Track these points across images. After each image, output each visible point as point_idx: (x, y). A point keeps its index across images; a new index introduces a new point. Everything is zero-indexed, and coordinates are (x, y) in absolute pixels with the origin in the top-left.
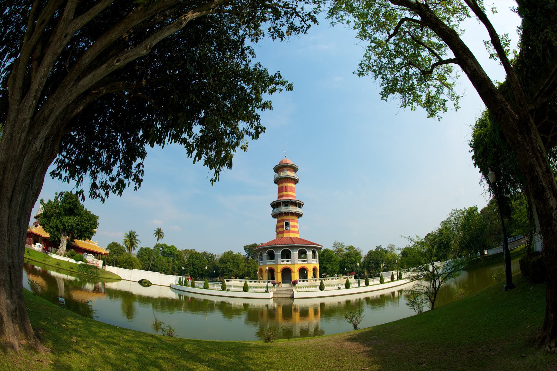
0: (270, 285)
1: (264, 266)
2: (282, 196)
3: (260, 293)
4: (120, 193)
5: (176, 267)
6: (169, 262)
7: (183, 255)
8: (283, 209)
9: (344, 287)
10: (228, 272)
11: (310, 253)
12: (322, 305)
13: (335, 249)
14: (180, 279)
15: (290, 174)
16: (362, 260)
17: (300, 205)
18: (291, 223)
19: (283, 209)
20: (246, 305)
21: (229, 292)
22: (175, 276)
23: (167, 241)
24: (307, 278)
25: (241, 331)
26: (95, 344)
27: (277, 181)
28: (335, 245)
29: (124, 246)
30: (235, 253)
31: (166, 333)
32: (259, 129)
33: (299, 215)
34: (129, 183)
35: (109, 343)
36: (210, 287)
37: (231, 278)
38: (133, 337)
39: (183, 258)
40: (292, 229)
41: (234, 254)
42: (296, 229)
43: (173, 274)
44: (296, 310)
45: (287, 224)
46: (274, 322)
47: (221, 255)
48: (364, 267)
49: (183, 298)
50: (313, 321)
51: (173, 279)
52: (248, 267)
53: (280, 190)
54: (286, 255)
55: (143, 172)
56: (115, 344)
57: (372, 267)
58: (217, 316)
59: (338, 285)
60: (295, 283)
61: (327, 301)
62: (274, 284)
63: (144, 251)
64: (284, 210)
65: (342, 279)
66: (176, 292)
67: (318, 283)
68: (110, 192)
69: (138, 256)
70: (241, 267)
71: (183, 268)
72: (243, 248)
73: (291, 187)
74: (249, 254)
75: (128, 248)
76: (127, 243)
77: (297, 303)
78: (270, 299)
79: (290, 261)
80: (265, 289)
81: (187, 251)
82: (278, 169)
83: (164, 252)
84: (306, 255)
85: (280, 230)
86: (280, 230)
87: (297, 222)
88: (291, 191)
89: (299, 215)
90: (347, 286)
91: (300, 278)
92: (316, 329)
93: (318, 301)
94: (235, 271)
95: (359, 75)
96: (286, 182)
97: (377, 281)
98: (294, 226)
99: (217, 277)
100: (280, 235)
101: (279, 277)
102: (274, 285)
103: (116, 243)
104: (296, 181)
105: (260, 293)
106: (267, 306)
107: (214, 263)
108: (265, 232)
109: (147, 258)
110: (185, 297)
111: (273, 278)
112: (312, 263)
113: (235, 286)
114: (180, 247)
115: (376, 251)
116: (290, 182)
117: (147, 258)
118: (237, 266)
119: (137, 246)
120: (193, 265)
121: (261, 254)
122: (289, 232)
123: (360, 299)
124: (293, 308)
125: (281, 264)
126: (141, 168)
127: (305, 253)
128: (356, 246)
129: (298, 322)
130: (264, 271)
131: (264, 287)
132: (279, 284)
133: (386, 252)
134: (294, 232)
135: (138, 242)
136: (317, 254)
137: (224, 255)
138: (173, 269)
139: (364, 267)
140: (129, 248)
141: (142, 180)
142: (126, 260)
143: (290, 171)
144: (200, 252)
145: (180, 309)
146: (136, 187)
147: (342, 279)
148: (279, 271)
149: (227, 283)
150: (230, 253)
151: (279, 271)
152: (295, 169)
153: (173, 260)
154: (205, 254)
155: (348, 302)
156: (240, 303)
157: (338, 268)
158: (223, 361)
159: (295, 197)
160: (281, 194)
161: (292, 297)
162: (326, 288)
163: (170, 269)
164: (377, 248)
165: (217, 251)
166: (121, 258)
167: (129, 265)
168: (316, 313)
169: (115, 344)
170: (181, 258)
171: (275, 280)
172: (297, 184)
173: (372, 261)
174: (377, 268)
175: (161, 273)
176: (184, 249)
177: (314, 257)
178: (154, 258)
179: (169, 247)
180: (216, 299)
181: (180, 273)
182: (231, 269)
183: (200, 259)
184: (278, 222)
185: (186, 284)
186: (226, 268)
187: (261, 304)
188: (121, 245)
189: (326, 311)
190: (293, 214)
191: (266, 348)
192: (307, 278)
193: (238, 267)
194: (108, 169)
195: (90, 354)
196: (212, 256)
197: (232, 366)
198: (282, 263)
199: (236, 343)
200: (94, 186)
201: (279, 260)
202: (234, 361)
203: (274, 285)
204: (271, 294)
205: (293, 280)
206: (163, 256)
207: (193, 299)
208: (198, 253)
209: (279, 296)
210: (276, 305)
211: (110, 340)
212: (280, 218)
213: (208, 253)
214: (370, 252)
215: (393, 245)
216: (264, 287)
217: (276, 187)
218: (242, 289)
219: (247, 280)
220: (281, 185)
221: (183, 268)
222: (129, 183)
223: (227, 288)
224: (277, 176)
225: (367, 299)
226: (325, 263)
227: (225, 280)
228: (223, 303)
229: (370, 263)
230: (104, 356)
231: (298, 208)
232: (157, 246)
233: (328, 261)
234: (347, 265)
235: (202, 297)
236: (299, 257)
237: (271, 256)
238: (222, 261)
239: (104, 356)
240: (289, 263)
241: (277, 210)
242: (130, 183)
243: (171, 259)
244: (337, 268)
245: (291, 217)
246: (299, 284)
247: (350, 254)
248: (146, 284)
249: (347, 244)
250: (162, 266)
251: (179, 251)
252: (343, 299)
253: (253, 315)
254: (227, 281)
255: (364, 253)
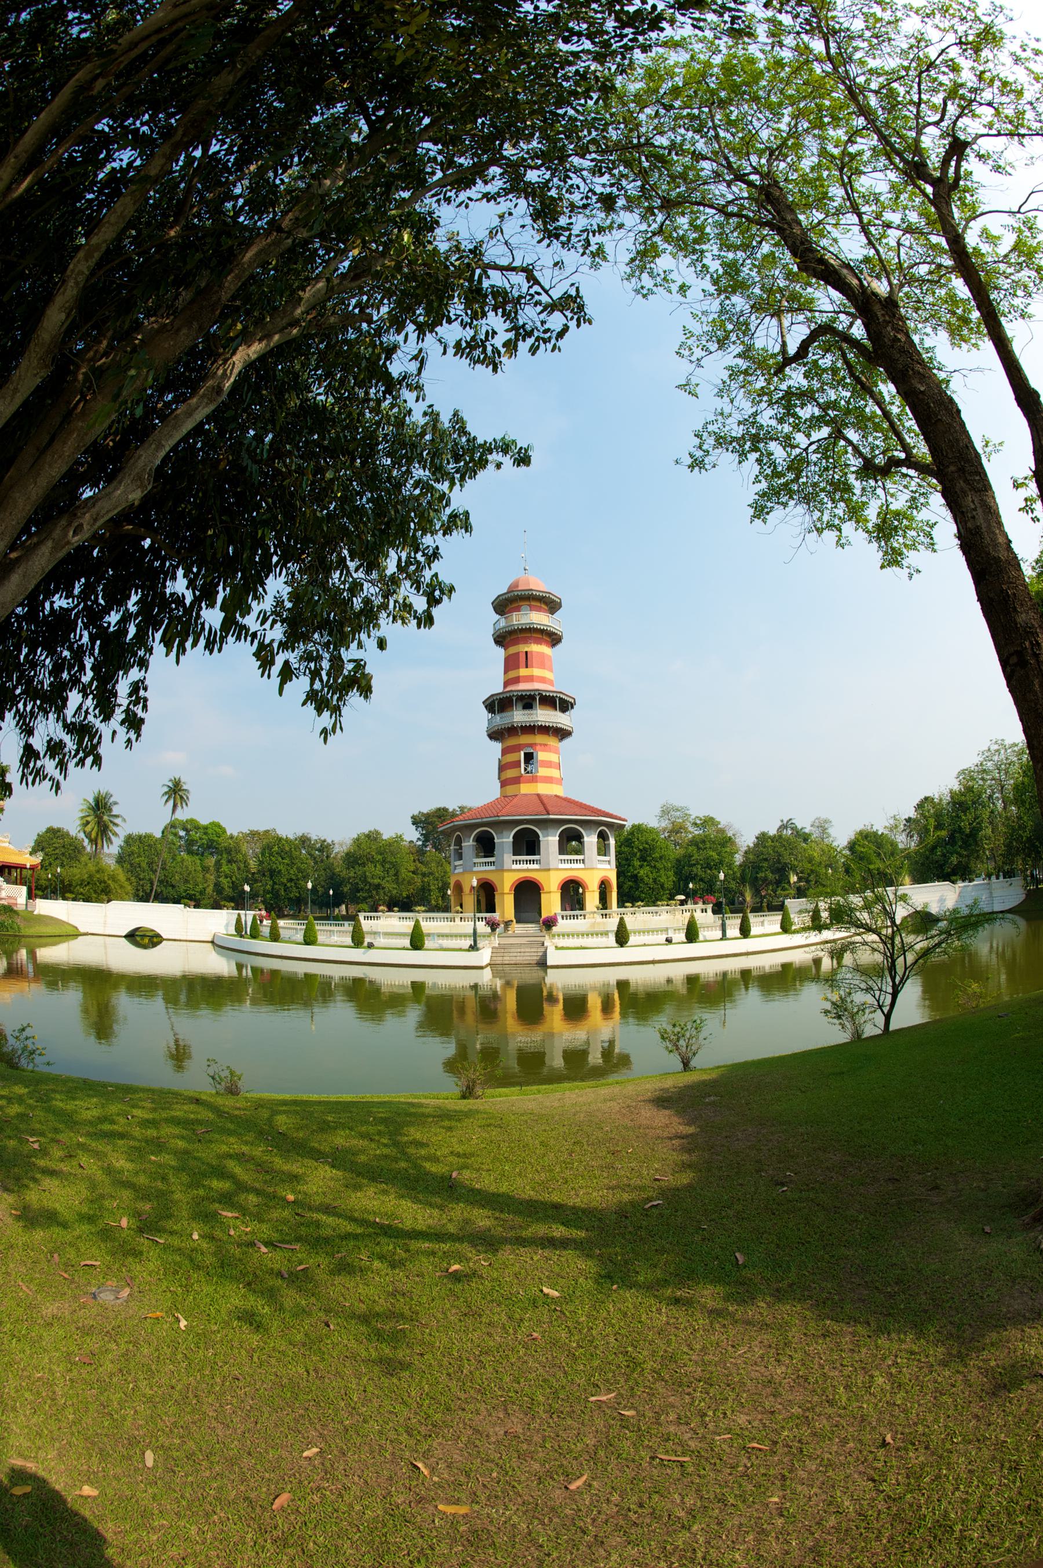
0: (482, 927)
1: (467, 876)
2: (517, 680)
3: (458, 952)
4: (98, 761)
5: (225, 882)
6: (205, 869)
7: (244, 847)
8: (519, 716)
9: (681, 936)
10: (369, 891)
11: (591, 840)
12: (622, 985)
13: (665, 824)
14: (238, 920)
15: (538, 618)
16: (738, 859)
17: (565, 705)
18: (541, 756)
19: (519, 716)
20: (418, 987)
21: (372, 951)
22: (224, 912)
23: (199, 811)
24: (582, 908)
25: (408, 1063)
26: (81, 1146)
27: (502, 639)
28: (665, 812)
29: (82, 835)
30: (387, 835)
31: (221, 1088)
32: (437, 593)
33: (562, 734)
34: (114, 732)
35: (110, 1136)
36: (321, 938)
37: (376, 911)
38: (154, 1110)
39: (244, 855)
40: (542, 772)
41: (385, 837)
42: (554, 773)
43: (216, 906)
44: (552, 999)
45: (529, 757)
46: (496, 1034)
47: (349, 842)
48: (743, 880)
49: (247, 973)
50: (601, 1029)
51: (219, 922)
52: (424, 875)
53: (511, 663)
54: (527, 844)
55: (146, 700)
56: (122, 1136)
57: (765, 880)
58: (341, 1013)
59: (667, 930)
60: (549, 924)
61: (638, 977)
62: (493, 925)
63: (137, 843)
64: (521, 718)
65: (678, 915)
66: (228, 958)
67: (613, 924)
68: (71, 765)
69: (120, 860)
70: (404, 874)
71: (247, 888)
72: (410, 821)
73: (542, 655)
74: (426, 838)
75: (91, 841)
76: (88, 828)
77: (555, 980)
78: (481, 968)
79: (538, 862)
80: (470, 942)
81: (253, 834)
82: (504, 605)
83: (190, 843)
84: (581, 843)
85: (510, 773)
86: (510, 773)
87: (557, 751)
88: (542, 666)
89: (562, 734)
90: (692, 934)
91: (563, 909)
92: (607, 1053)
93: (613, 976)
94: (389, 885)
95: (691, 467)
96: (525, 641)
97: (771, 922)
98: (548, 764)
99: (338, 905)
100: (510, 790)
101: (506, 905)
102: (493, 930)
103: (59, 830)
104: (554, 639)
105: (458, 952)
106: (475, 987)
107: (329, 867)
108: (471, 783)
109: (144, 865)
110: (254, 970)
111: (491, 908)
112: (597, 867)
113: (387, 934)
114: (235, 826)
115: (778, 838)
116: (538, 641)
117: (144, 865)
118: (392, 872)
119: (116, 834)
120: (273, 873)
121: (459, 842)
122: (534, 780)
123: (725, 974)
124: (545, 993)
125: (511, 870)
126: (142, 693)
127: (579, 838)
128: (723, 819)
129: (560, 1033)
130: (466, 889)
131: (465, 936)
132: (507, 924)
133: (806, 838)
134: (549, 780)
135: (117, 821)
136: (612, 842)
137: (357, 841)
138: (218, 888)
139: (743, 880)
140: (93, 841)
141: (142, 721)
142: (91, 876)
143: (539, 609)
144: (291, 837)
145: (240, 1000)
146: (129, 741)
147: (678, 915)
148: (507, 889)
149: (366, 924)
150: (373, 837)
151: (507, 889)
152: (552, 605)
153: (218, 864)
154: (304, 840)
155: (692, 980)
156: (403, 979)
157: (673, 878)
158: (363, 1151)
159: (551, 683)
160: (512, 674)
161: (542, 964)
162: (633, 939)
163: (210, 890)
164: (783, 827)
165: (339, 830)
166: (76, 872)
167: (97, 890)
168: (607, 1007)
169: (122, 1136)
170: (240, 857)
171: (496, 916)
172: (559, 647)
173: (765, 864)
174: (778, 883)
175: (186, 905)
176: (246, 831)
177: (603, 850)
178: (164, 863)
179: (206, 828)
180: (336, 972)
181: (238, 901)
182: (376, 881)
183: (291, 858)
184: (505, 752)
185: (255, 935)
186: (364, 879)
187: (461, 980)
188: (73, 832)
189: (636, 1002)
190: (545, 730)
191: (469, 1114)
192: (582, 908)
193: (396, 875)
194: (54, 699)
195: (80, 1171)
196: (324, 847)
197: (383, 1163)
198: (514, 867)
199: (390, 1103)
200: (29, 753)
201: (508, 858)
202: (386, 1151)
203: (493, 930)
204: (484, 956)
205: (544, 915)
206: (190, 852)
207: (274, 973)
208: (287, 840)
209: (507, 959)
210: (499, 983)
211: (106, 1127)
212: (512, 742)
213: (314, 837)
214: (762, 838)
215: (826, 821)
216: (465, 936)
217: (499, 654)
218: (407, 942)
219: (420, 917)
220: (512, 650)
221: (247, 888)
222: (114, 732)
223: (367, 940)
224: (503, 623)
225: (745, 974)
226: (637, 863)
227: (361, 916)
228: (358, 981)
229: (760, 868)
230: (109, 1171)
231: (558, 713)
232: (173, 825)
233: (643, 859)
234: (697, 870)
235: (300, 969)
236: (562, 851)
237: (486, 846)
238: (353, 859)
239: (109, 1171)
240: (536, 866)
241: (501, 720)
242: (111, 732)
243: (211, 861)
244: (668, 879)
245: (539, 739)
246: (563, 925)
247: (704, 842)
248: (146, 940)
249: (698, 811)
250: (186, 881)
251: (232, 837)
252: (679, 972)
253: (439, 1011)
254: (366, 918)
255: (746, 840)
